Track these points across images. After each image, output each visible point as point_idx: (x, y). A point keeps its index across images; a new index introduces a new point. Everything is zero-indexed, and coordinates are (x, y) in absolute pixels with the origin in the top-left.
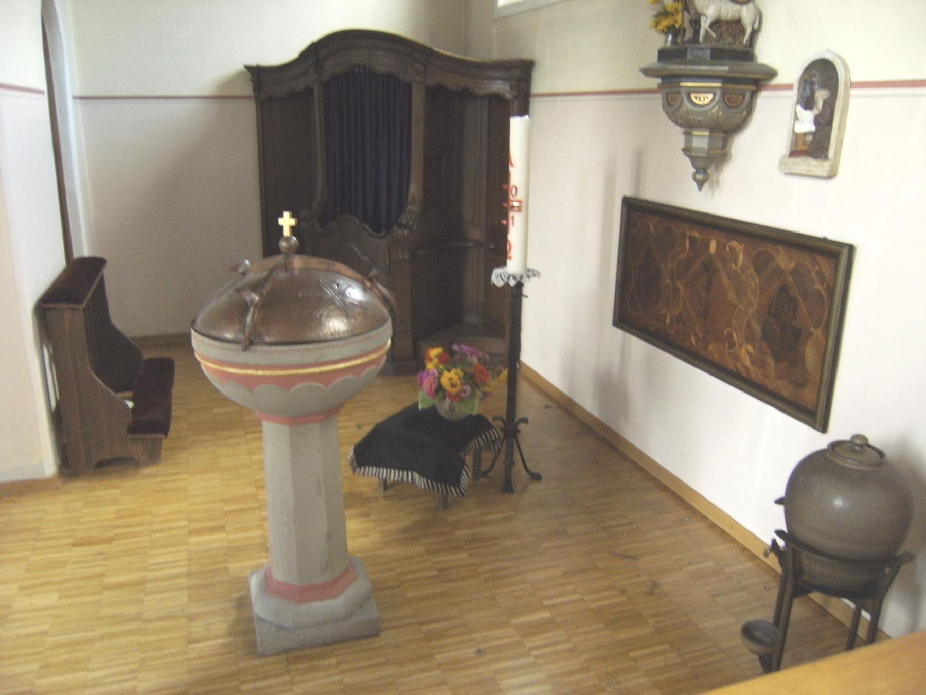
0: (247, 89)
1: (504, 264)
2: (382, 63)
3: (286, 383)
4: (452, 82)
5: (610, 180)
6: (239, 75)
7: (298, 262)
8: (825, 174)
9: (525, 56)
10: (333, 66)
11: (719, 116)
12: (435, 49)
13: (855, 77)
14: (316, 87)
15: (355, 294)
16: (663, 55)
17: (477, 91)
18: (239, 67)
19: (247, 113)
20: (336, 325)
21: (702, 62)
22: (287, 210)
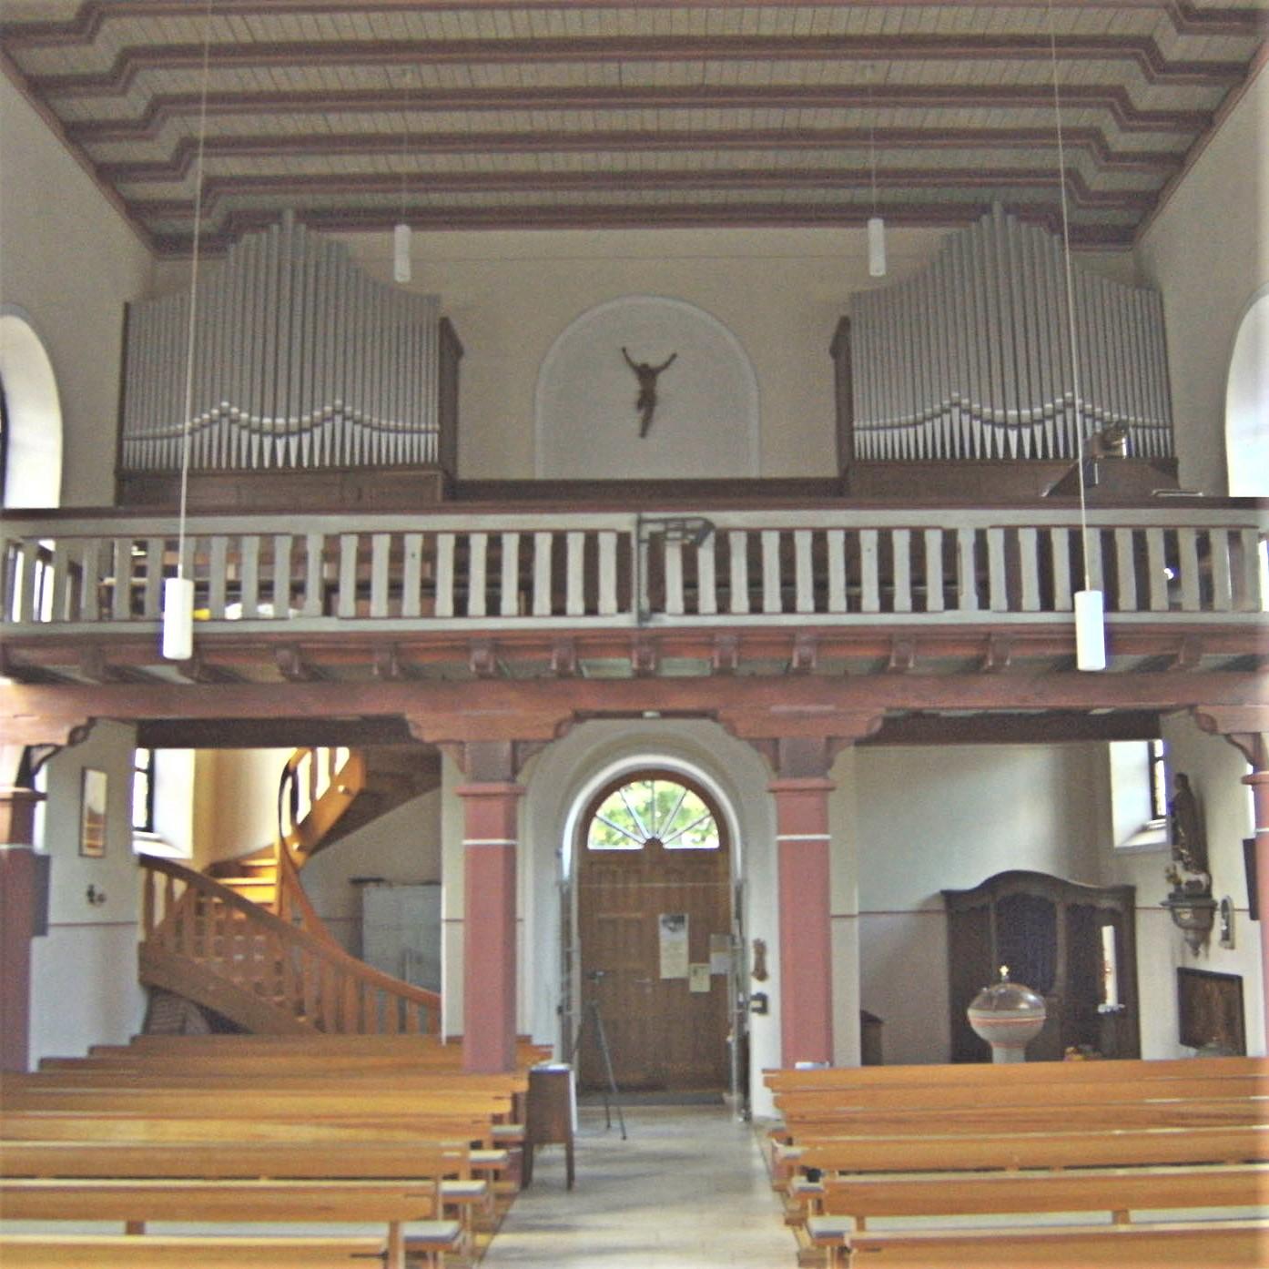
0: (940, 905)
1: (1104, 1002)
2: (1036, 891)
3: (1007, 1024)
4: (1081, 902)
5: (1173, 960)
6: (935, 896)
7: (1009, 986)
8: (371, 888)
9: (1131, 883)
10: (1004, 892)
11: (1193, 921)
12: (1070, 881)
13: (1236, 907)
14: (992, 906)
15: (1031, 997)
16: (1171, 896)
17: (1098, 906)
18: (937, 890)
19: (940, 924)
20: (1023, 1006)
21: (1182, 901)
22: (1007, 966)
